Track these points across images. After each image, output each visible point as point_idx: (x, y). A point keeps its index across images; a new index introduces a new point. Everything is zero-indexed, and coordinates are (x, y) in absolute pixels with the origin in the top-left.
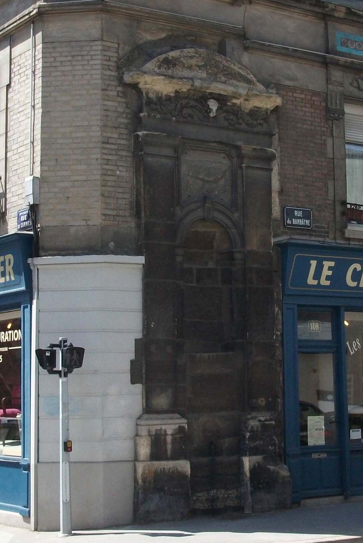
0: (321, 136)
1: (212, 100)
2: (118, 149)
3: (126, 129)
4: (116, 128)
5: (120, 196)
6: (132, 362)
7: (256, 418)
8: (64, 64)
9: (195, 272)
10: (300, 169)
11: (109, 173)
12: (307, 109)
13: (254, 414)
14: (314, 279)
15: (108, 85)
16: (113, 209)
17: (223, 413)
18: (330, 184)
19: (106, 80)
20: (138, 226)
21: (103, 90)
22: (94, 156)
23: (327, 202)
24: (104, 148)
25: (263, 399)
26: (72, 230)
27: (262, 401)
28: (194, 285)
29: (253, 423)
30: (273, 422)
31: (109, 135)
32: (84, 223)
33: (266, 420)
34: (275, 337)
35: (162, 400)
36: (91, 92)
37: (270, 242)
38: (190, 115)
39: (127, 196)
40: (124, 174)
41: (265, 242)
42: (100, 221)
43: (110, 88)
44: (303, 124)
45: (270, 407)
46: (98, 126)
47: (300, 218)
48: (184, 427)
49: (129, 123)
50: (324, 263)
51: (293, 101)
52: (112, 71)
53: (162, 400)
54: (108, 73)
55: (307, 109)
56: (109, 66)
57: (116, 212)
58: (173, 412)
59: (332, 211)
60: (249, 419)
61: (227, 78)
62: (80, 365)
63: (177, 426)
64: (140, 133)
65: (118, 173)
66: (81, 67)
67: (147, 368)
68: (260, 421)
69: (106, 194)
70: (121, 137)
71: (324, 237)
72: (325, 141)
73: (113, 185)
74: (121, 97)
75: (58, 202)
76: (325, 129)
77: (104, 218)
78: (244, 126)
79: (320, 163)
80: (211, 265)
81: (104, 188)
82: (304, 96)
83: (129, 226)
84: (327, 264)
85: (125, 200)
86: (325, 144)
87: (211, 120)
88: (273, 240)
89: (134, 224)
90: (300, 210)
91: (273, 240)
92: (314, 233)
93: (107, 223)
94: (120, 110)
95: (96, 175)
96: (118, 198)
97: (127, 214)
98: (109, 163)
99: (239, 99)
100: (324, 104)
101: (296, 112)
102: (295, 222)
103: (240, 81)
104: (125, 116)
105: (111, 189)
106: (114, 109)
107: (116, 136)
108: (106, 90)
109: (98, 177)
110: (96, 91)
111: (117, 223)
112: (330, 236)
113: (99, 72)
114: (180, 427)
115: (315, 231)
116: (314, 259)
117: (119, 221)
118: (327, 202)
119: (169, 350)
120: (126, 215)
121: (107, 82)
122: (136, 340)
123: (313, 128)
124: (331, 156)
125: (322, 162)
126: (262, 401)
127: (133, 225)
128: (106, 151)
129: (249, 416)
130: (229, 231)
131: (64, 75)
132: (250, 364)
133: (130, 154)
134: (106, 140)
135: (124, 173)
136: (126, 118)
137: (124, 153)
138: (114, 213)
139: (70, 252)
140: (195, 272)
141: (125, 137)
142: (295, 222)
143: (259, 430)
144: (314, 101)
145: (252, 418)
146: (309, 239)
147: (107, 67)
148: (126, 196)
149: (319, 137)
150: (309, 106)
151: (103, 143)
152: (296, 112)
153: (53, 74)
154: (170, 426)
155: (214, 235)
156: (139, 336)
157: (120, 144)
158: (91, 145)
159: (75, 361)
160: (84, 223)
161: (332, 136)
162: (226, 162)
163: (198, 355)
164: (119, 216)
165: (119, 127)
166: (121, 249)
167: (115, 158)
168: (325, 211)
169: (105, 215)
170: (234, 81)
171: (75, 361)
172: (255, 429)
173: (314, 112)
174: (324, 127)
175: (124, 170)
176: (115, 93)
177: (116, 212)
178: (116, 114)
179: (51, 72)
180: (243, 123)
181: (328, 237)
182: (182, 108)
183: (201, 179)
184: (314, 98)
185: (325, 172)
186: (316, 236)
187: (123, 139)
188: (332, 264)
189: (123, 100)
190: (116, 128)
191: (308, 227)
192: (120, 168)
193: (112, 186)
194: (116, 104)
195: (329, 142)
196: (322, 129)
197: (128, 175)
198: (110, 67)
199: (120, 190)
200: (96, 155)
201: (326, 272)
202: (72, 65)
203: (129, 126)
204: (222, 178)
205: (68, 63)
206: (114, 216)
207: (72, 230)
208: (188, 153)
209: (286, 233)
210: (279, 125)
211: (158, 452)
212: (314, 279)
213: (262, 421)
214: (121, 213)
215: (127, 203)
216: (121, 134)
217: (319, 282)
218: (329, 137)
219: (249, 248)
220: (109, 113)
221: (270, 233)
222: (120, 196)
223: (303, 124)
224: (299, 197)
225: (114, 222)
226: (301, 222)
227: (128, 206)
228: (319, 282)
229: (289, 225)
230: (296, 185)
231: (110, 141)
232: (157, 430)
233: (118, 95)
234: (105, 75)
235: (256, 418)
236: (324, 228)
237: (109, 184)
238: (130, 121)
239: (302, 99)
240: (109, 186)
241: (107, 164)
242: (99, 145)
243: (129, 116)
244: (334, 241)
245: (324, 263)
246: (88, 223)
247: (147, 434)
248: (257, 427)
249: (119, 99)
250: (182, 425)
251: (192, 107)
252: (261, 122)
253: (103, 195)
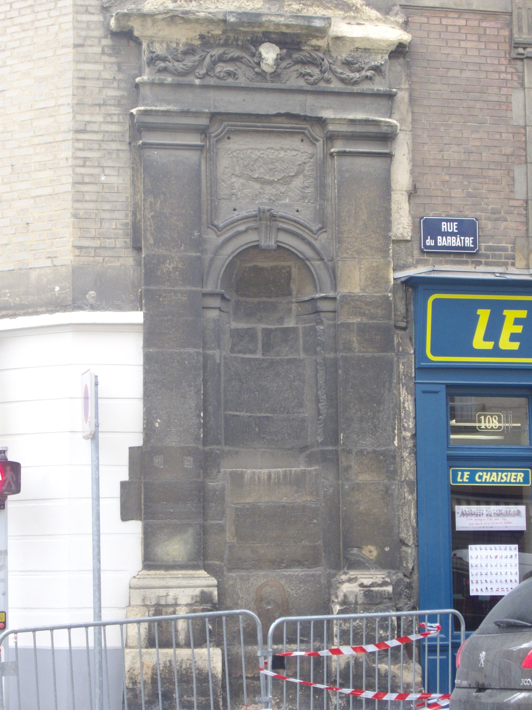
0: (500, 88)
1: (267, 45)
2: (103, 141)
3: (119, 105)
4: (99, 105)
5: (106, 215)
6: (123, 485)
7: (355, 579)
8: (23, 12)
9: (260, 335)
10: (455, 148)
11: (87, 180)
12: (469, 45)
13: (352, 573)
14: (486, 338)
15: (86, 38)
16: (93, 238)
17: (298, 572)
18: (519, 172)
19: (82, 29)
20: (138, 263)
21: (76, 46)
22: (63, 155)
23: (512, 203)
24: (78, 140)
25: (372, 548)
26: (34, 275)
27: (371, 552)
28: (259, 356)
29: (346, 588)
30: (390, 589)
31: (87, 118)
32: (48, 263)
33: (372, 585)
34: (396, 442)
35: (175, 548)
36: (59, 52)
37: (387, 282)
38: (229, 74)
39: (120, 215)
40: (114, 180)
41: (377, 278)
42: (72, 258)
43: (89, 42)
44: (461, 70)
45: (383, 563)
46: (68, 104)
47: (452, 234)
48: (210, 595)
49: (122, 97)
50: (506, 312)
51: (440, 33)
52: (92, 14)
53: (175, 548)
54: (85, 18)
55: (469, 45)
56: (87, 6)
57: (99, 242)
58: (195, 567)
59: (523, 219)
60: (342, 582)
61: (304, 4)
62: (18, 490)
63: (197, 591)
64: (134, 111)
65: (103, 178)
66: (45, 15)
67: (152, 494)
68: (362, 585)
69: (81, 213)
70: (109, 119)
71: (505, 264)
72: (508, 96)
73: (94, 198)
74: (110, 55)
75: (13, 232)
76: (509, 77)
77: (77, 252)
78: (335, 85)
79: (497, 136)
80: (290, 323)
81: (78, 205)
82: (463, 22)
83: (124, 262)
84: (510, 315)
85: (115, 223)
86: (508, 103)
87: (268, 77)
88: (392, 275)
89: (131, 259)
90: (453, 221)
91: (392, 275)
92: (483, 261)
93: (84, 259)
94: (107, 75)
95: (66, 184)
96: (102, 220)
97: (119, 243)
98: (88, 163)
99: (323, 38)
100: (506, 33)
101: (448, 51)
102: (442, 241)
103: (329, 8)
104: (115, 84)
105: (91, 206)
106: (96, 75)
107: (100, 119)
108: (82, 46)
109: (69, 187)
110: (65, 50)
111: (101, 259)
112: (517, 265)
113: (70, 18)
114: (202, 593)
115: (487, 257)
116: (484, 304)
117: (104, 257)
118: (512, 203)
119: (189, 463)
120: (118, 246)
121: (83, 33)
122: (131, 449)
123: (483, 75)
124: (521, 123)
125: (500, 133)
126: (371, 552)
127: (130, 261)
128: (80, 145)
129: (344, 577)
130: (308, 263)
131: (23, 30)
132: (347, 487)
133: (125, 147)
134: (82, 127)
135: (117, 179)
136: (119, 88)
137: (114, 146)
138: (97, 243)
139: (30, 310)
140: (260, 335)
141: (115, 119)
142: (442, 241)
143: (360, 601)
144: (485, 29)
145: (350, 580)
146: (474, 270)
147: (85, 8)
148: (116, 215)
149: (496, 90)
150: (475, 38)
151: (77, 131)
152: (448, 51)
153: (9, 31)
154: (185, 588)
155: (289, 273)
156: (138, 441)
157: (107, 132)
158: (60, 137)
159: (9, 484)
160: (48, 263)
161: (522, 85)
162: (306, 148)
163: (249, 471)
164: (105, 248)
165: (105, 104)
166: (107, 300)
167: (96, 155)
168: (506, 220)
169: (80, 248)
170: (317, 9)
171: (9, 484)
172: (351, 599)
173: (486, 48)
174: (506, 72)
175: (113, 173)
176: (99, 50)
177: (99, 242)
178: (101, 83)
179: (6, 27)
180: (334, 79)
181: (513, 264)
182: (214, 63)
183: (257, 180)
184: (484, 24)
185: (508, 150)
186: (487, 264)
187: (113, 123)
188: (523, 314)
189: (113, 60)
190: (99, 105)
191: (469, 248)
192: (107, 171)
193: (92, 201)
194: (101, 67)
195: (517, 97)
196: (503, 76)
197: (121, 181)
198: (91, 9)
199: (107, 206)
200: (66, 152)
201: (509, 328)
202: (34, 12)
203: (124, 102)
204: (296, 175)
205: (29, 11)
206: (96, 248)
207: (34, 275)
208: (231, 137)
209: (424, 263)
210: (409, 76)
211: (159, 635)
212: (486, 338)
213: (366, 586)
214: (108, 243)
215: (118, 226)
216: (109, 115)
217: (496, 346)
218: (516, 88)
219: (343, 290)
220: (87, 83)
221: (388, 264)
222: (106, 215)
223: (461, 70)
224: (452, 197)
225: (97, 259)
226: (454, 241)
227: (121, 232)
228: (496, 346)
229: (430, 247)
230: (447, 178)
231: (89, 128)
232: (159, 597)
233: (103, 53)
234: (79, 22)
235: (355, 579)
236: (504, 249)
237: (87, 198)
238: (125, 94)
239: (460, 27)
240: (86, 201)
241: (83, 166)
242: (70, 136)
243: (123, 85)
244: (526, 272)
245: (506, 312)
246: (56, 263)
247: (139, 602)
248: (356, 596)
249: (105, 58)
250: (206, 589)
251: (233, 60)
252: (369, 73)
253: (75, 216)
